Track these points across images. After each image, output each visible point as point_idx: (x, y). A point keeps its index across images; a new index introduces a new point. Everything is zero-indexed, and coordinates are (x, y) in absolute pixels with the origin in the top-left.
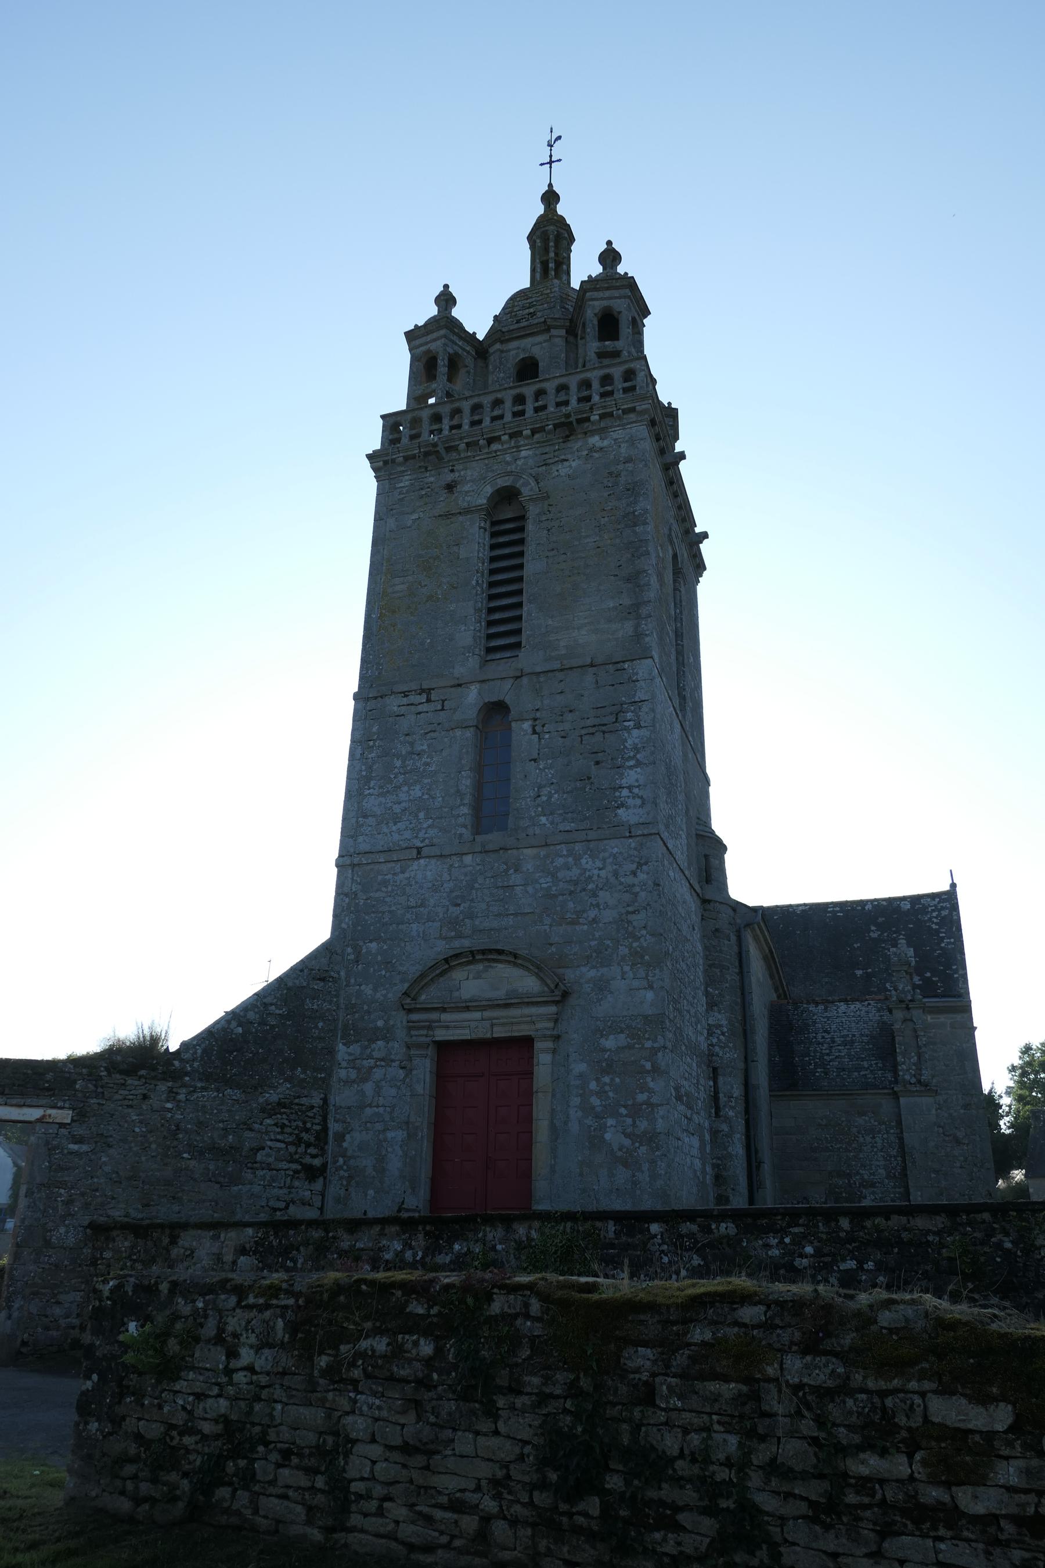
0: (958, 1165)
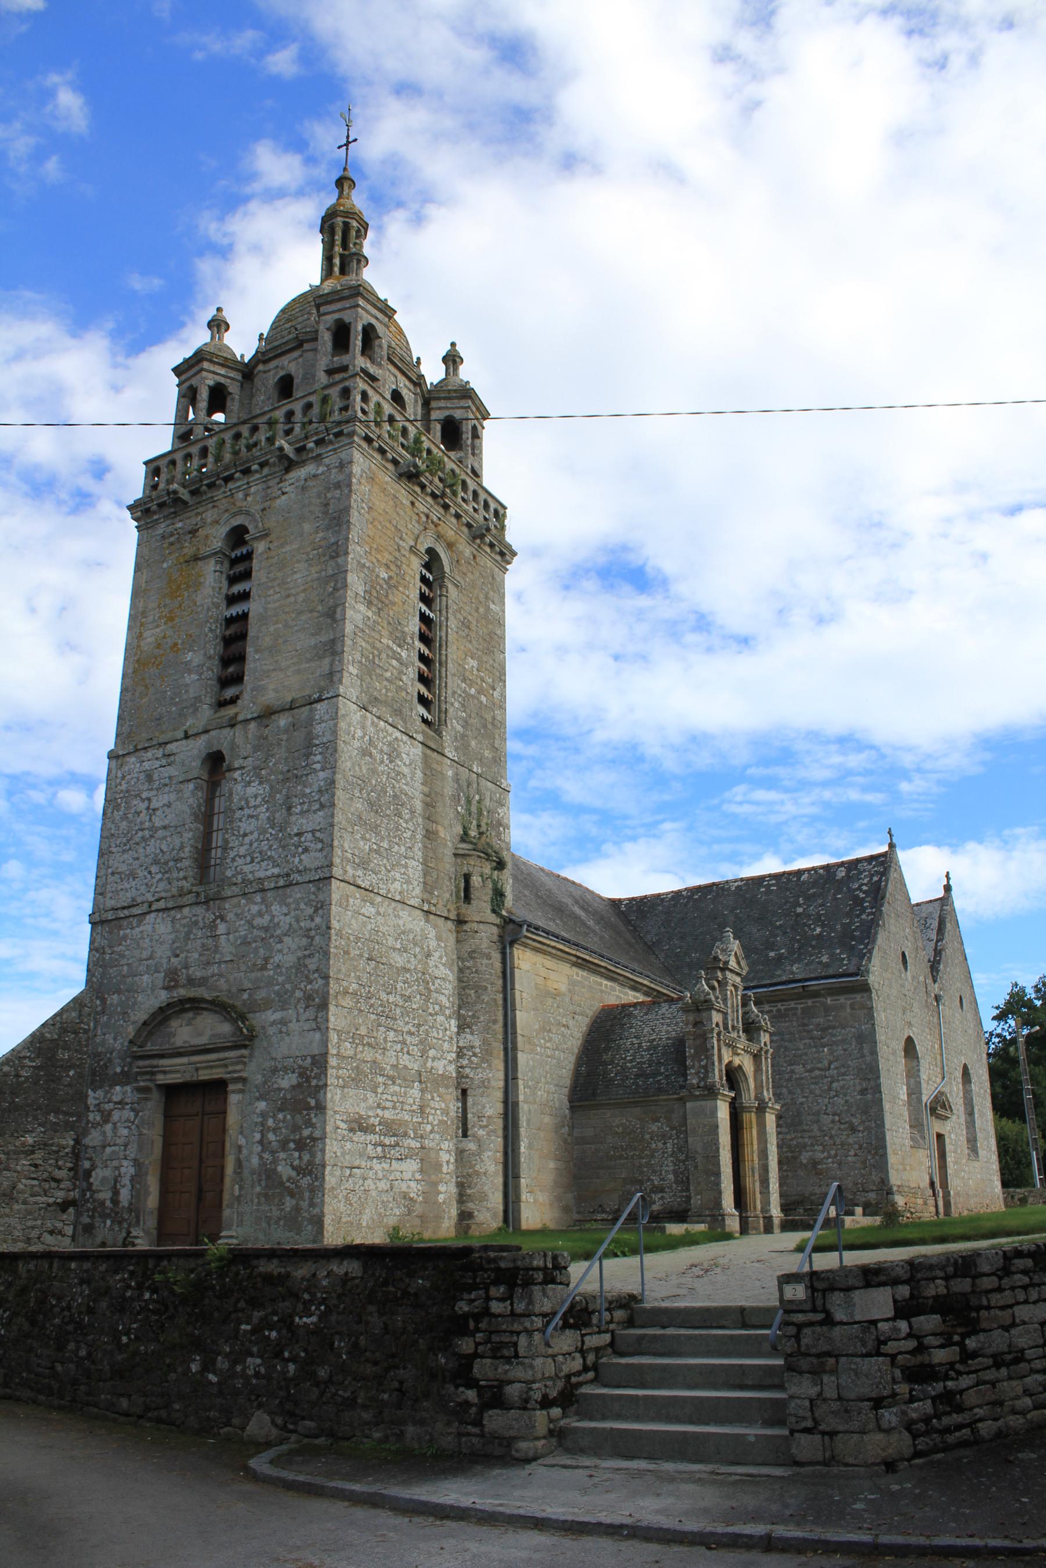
0: (852, 1153)
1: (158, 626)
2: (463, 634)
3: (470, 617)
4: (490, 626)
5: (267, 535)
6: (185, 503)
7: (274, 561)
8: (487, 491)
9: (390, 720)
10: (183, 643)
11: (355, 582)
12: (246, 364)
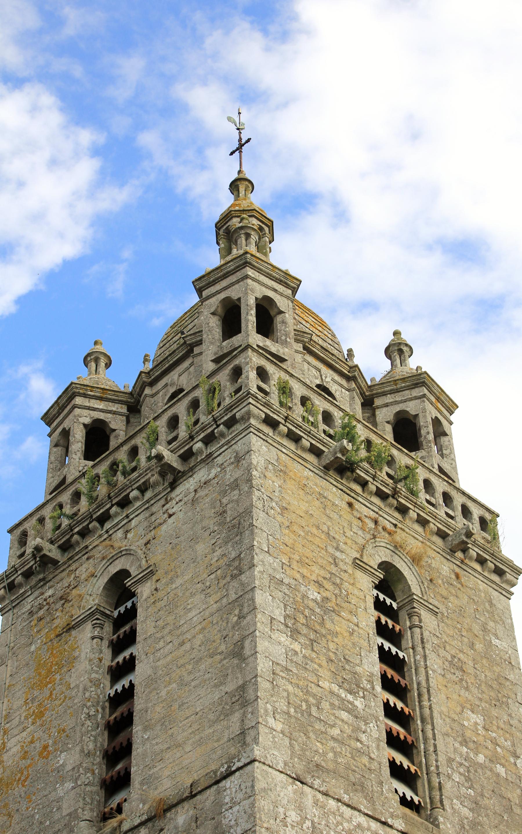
1: (24, 730)
2: (454, 678)
3: (461, 656)
4: (497, 669)
5: (152, 573)
6: (55, 562)
7: (162, 603)
8: (464, 493)
9: (346, 798)
10: (55, 743)
11: (268, 604)
12: (131, 394)
